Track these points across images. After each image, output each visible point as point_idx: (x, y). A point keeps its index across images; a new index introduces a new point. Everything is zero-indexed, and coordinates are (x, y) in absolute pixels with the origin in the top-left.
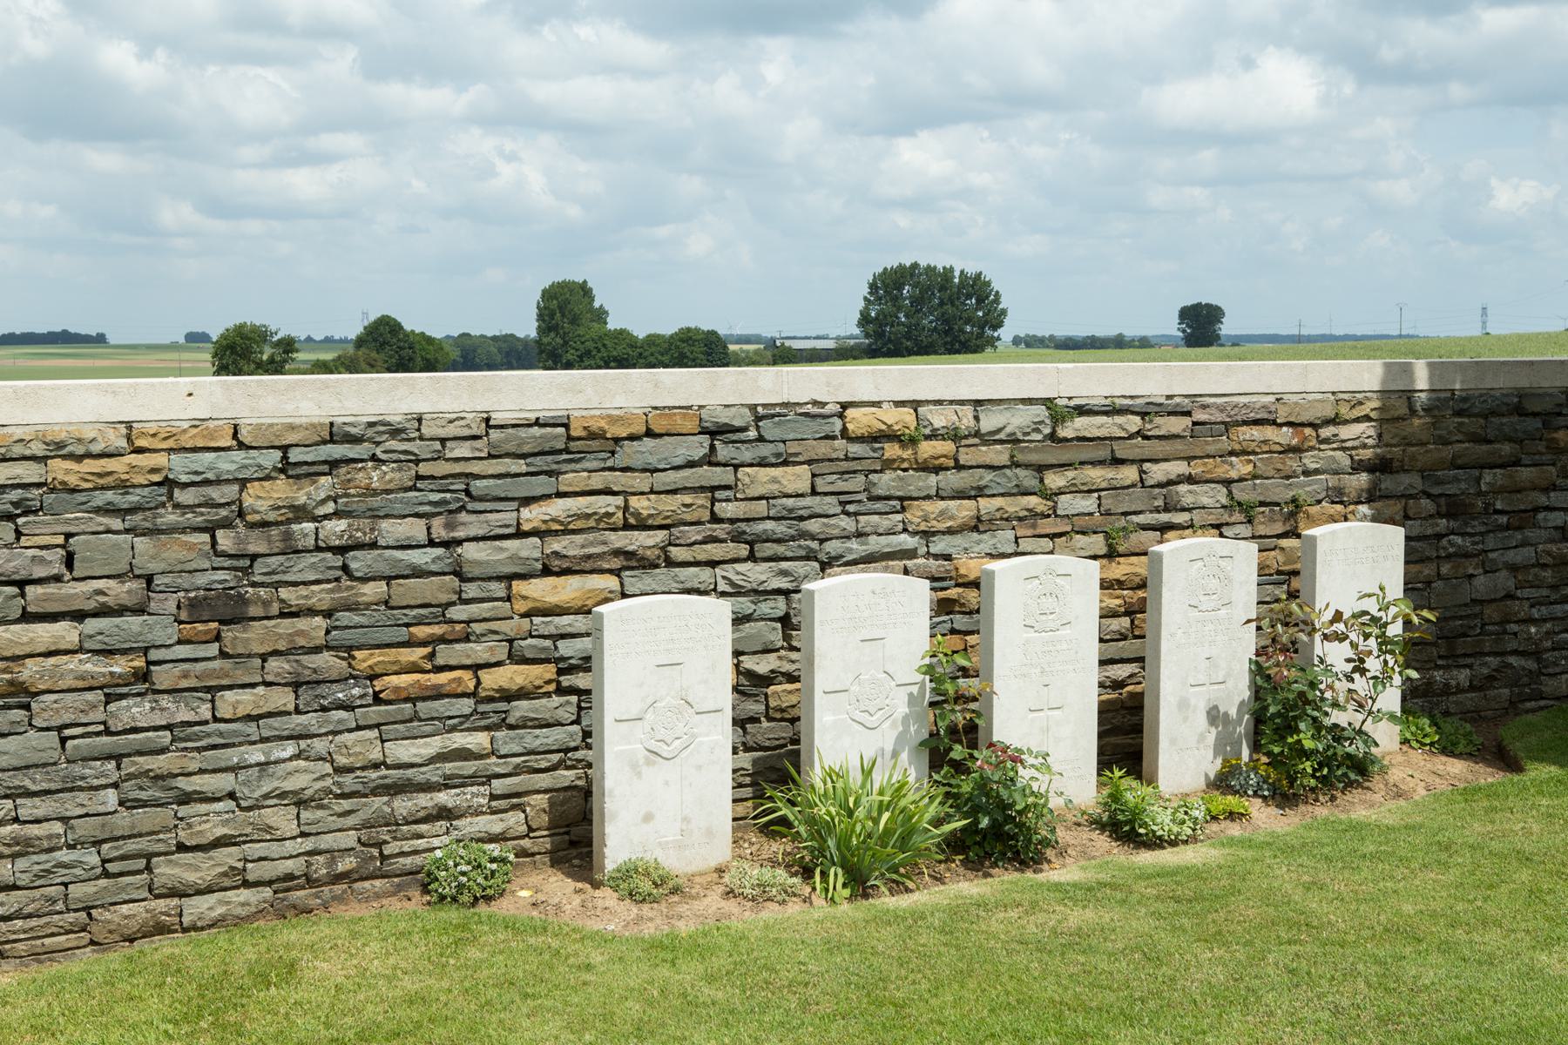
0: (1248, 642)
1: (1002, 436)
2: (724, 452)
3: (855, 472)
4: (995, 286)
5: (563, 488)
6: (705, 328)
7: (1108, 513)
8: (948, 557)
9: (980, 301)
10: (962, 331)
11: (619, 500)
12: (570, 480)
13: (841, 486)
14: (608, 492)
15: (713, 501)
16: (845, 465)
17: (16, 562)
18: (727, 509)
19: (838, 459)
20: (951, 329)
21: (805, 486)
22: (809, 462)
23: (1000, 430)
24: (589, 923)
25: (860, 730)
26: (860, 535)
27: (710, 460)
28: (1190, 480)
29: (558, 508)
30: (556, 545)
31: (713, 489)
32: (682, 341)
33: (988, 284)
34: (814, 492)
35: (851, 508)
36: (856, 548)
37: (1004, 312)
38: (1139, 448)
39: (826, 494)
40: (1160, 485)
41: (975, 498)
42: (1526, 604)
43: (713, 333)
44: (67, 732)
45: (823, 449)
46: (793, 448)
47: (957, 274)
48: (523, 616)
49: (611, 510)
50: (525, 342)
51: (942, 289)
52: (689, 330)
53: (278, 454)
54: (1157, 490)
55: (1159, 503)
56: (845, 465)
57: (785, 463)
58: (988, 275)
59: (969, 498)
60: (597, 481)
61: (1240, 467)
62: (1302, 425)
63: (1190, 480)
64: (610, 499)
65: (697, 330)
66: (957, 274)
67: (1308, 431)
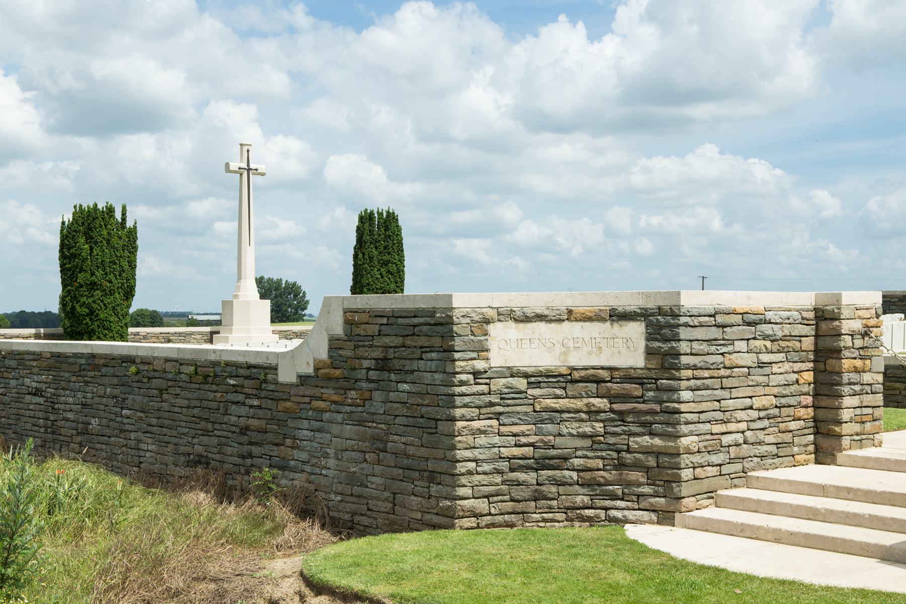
0: (762, 575)
4: (303, 289)
6: (151, 309)
9: (296, 296)
10: (287, 310)
20: (280, 310)
24: (470, 576)
32: (138, 315)
33: (300, 287)
37: (307, 302)
42: (801, 381)
43: (155, 312)
44: (434, 431)
47: (284, 282)
50: (54, 315)
51: (277, 289)
52: (142, 310)
53: (193, 368)
58: (299, 283)
65: (147, 310)
66: (284, 282)
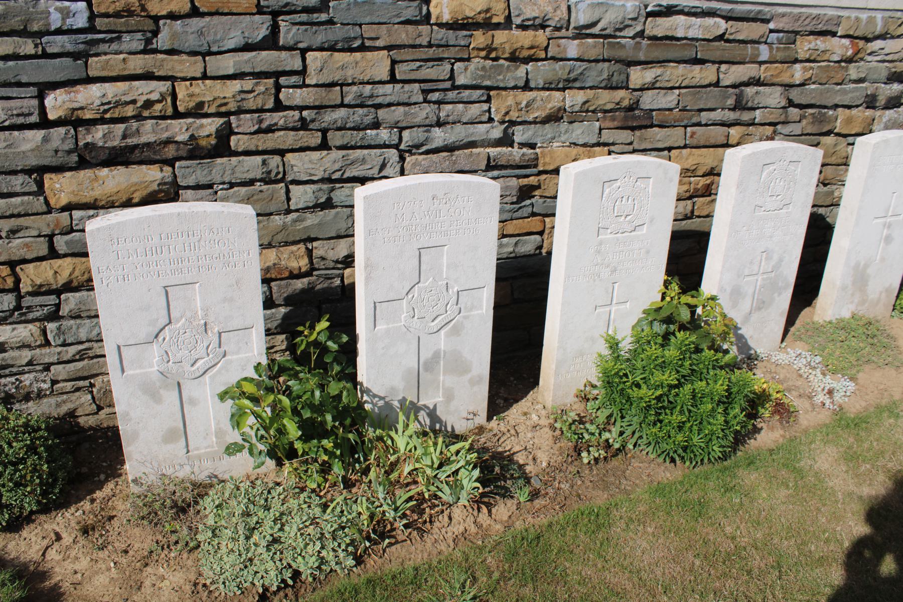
1: (596, 30)
2: (288, 33)
3: (441, 59)
5: (92, 73)
7: (684, 110)
8: (533, 146)
11: (163, 87)
12: (96, 65)
13: (429, 72)
14: (148, 76)
15: (278, 88)
16: (431, 52)
17: (16, 247)
18: (296, 96)
19: (420, 46)
21: (383, 73)
22: (389, 48)
23: (594, 24)
25: (600, 300)
26: (439, 124)
27: (271, 42)
28: (757, 82)
29: (91, 96)
30: (97, 135)
31: (277, 74)
34: (393, 79)
35: (435, 96)
36: (439, 136)
38: (720, 50)
39: (247, 153)
40: (734, 86)
41: (563, 89)
45: (404, 35)
46: (368, 32)
48: (64, 209)
49: (155, 96)
54: (731, 90)
55: (731, 102)
56: (431, 52)
57: (362, 48)
59: (558, 90)
60: (137, 64)
61: (798, 73)
62: (857, 38)
63: (757, 82)
64: (154, 84)
67: (861, 43)
